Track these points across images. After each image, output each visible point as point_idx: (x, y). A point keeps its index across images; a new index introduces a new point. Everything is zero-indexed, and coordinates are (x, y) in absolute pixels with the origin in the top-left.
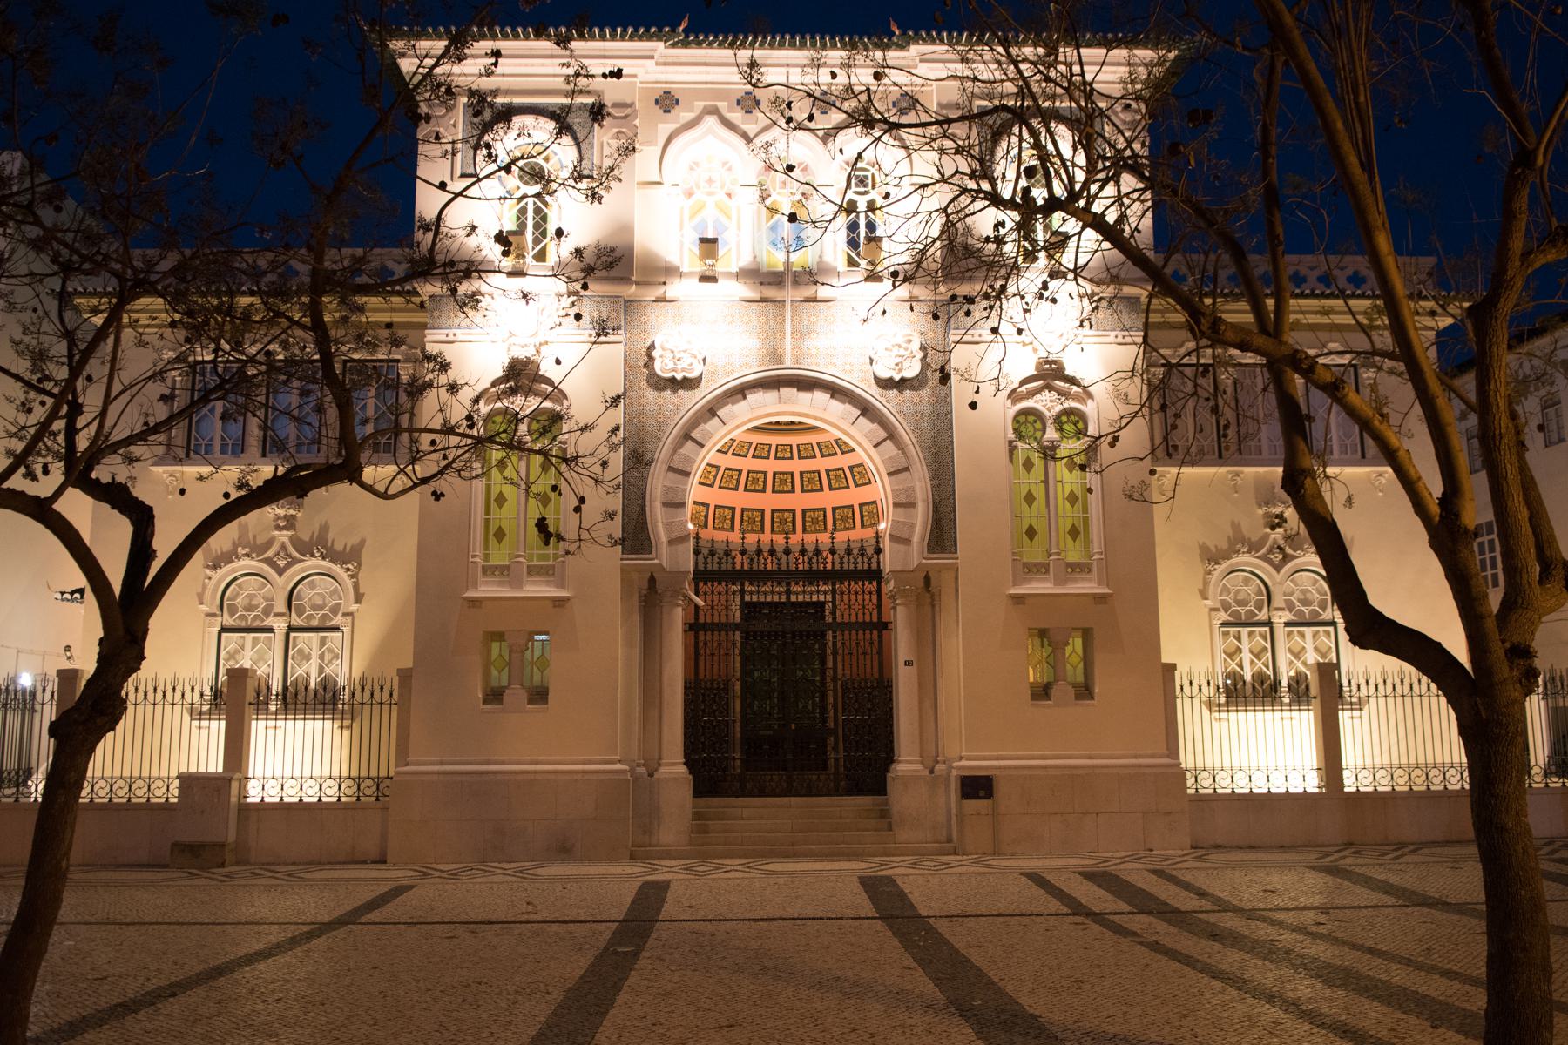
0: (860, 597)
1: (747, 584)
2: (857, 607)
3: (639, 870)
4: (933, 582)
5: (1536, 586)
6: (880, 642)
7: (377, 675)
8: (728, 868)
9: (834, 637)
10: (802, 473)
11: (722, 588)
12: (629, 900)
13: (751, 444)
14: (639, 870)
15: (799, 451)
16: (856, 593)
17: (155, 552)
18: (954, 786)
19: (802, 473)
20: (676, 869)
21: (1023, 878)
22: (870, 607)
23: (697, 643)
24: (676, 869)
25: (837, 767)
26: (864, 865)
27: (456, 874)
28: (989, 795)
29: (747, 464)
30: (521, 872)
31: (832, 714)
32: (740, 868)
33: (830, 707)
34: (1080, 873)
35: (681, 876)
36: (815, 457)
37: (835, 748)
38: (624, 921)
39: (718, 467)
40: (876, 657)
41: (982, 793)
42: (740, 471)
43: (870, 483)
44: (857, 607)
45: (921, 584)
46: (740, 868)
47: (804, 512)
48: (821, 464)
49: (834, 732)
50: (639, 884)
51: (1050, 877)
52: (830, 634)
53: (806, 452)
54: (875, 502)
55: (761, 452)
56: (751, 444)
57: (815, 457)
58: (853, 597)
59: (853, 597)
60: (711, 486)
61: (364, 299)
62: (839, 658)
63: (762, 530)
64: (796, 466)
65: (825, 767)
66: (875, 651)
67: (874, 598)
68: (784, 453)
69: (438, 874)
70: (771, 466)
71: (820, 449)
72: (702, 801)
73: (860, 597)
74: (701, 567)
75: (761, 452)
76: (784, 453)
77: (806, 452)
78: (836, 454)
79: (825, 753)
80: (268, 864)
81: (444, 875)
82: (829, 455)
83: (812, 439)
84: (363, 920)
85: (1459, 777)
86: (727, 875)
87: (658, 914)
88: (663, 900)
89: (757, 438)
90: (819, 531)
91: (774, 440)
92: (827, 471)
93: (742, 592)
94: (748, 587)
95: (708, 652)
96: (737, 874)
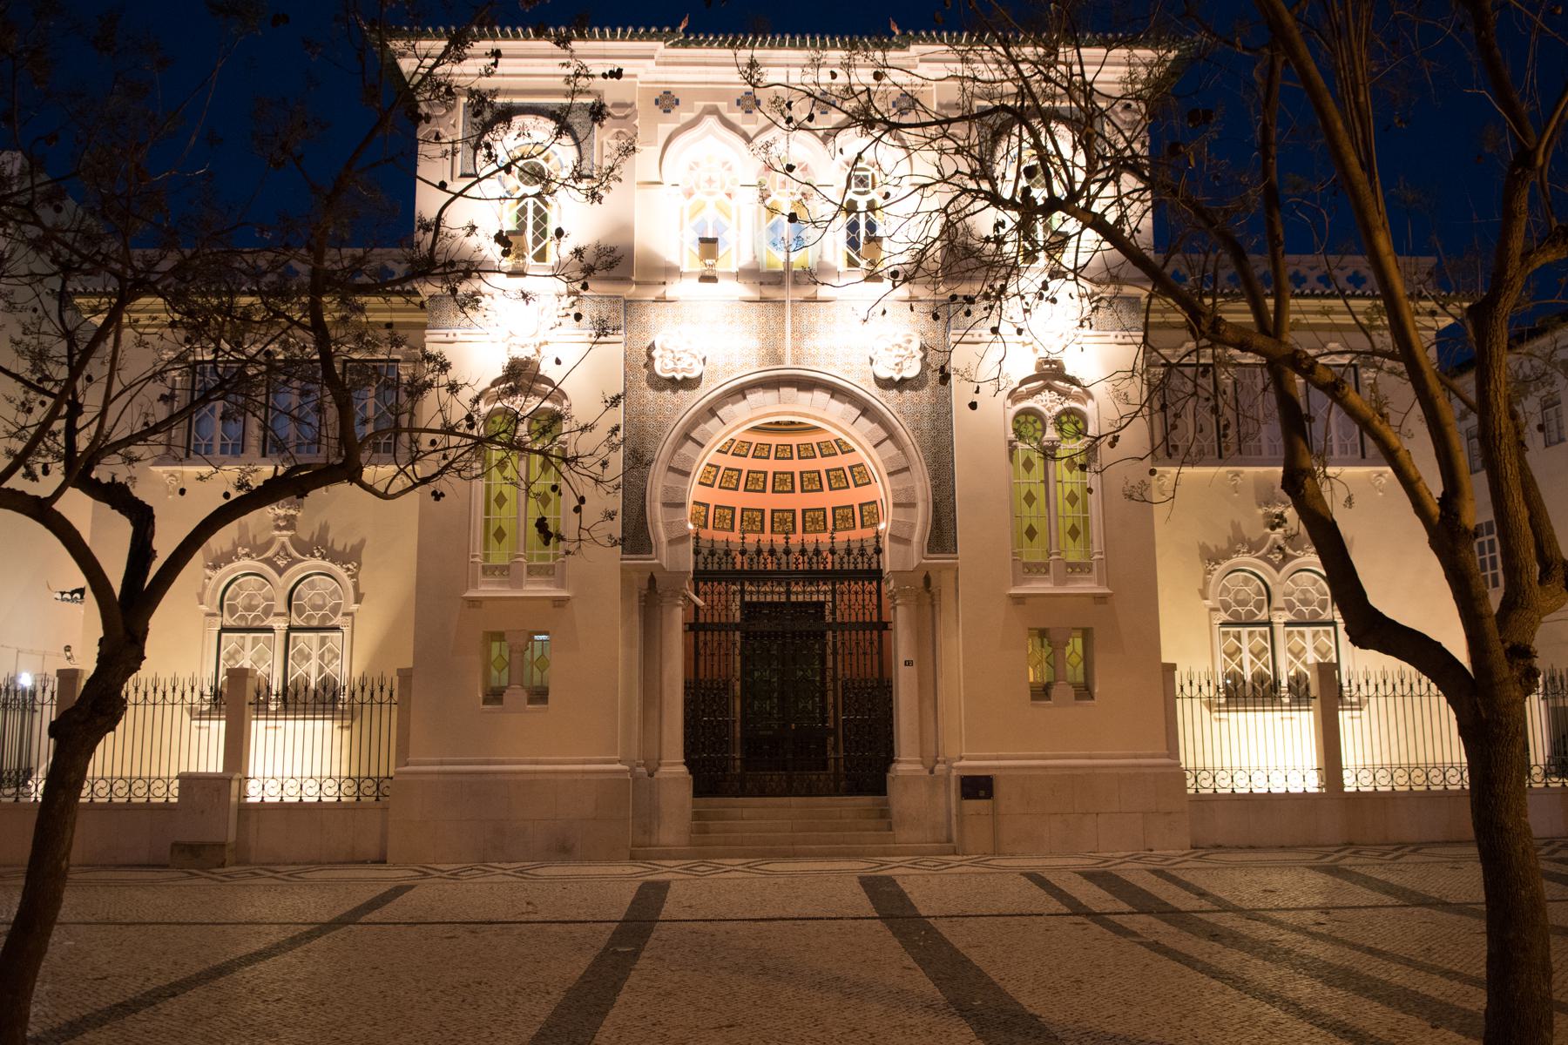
1: (747, 584)
2: (857, 607)
3: (639, 870)
4: (933, 582)
5: (1536, 586)
6: (880, 642)
7: (377, 675)
8: (728, 868)
9: (834, 637)
10: (802, 473)
12: (629, 900)
13: (751, 444)
14: (639, 870)
15: (799, 451)
16: (856, 593)
17: (155, 552)
18: (954, 786)
19: (802, 473)
20: (676, 869)
21: (1023, 878)
22: (870, 607)
23: (697, 643)
24: (676, 869)
26: (864, 865)
27: (456, 874)
28: (989, 795)
29: (747, 464)
30: (521, 872)
31: (832, 714)
32: (740, 868)
33: (830, 707)
34: (1080, 873)
35: (681, 876)
36: (815, 457)
37: (835, 748)
38: (624, 921)
39: (718, 467)
40: (876, 657)
41: (982, 793)
42: (740, 471)
43: (870, 483)
44: (857, 607)
45: (921, 584)
46: (740, 868)
47: (804, 512)
48: (821, 464)
49: (834, 732)
50: (639, 884)
51: (1050, 877)
52: (830, 634)
53: (806, 452)
54: (875, 502)
55: (761, 452)
56: (751, 444)
57: (815, 457)
59: (853, 597)
60: (711, 486)
61: (364, 299)
62: (839, 658)
63: (762, 530)
64: (796, 466)
65: (825, 767)
66: (875, 651)
67: (874, 598)
68: (784, 453)
69: (438, 874)
70: (771, 466)
71: (820, 449)
72: (702, 801)
73: (860, 597)
74: (701, 567)
75: (761, 452)
76: (784, 453)
77: (806, 452)
78: (836, 454)
79: (825, 753)
80: (268, 864)
81: (444, 875)
82: (829, 455)
83: (812, 439)
84: (363, 920)
85: (1459, 777)
86: (727, 875)
87: (658, 914)
88: (663, 900)
89: (757, 438)
91: (774, 440)
92: (827, 471)
93: (742, 592)
94: (748, 587)
95: (708, 652)
96: (737, 874)
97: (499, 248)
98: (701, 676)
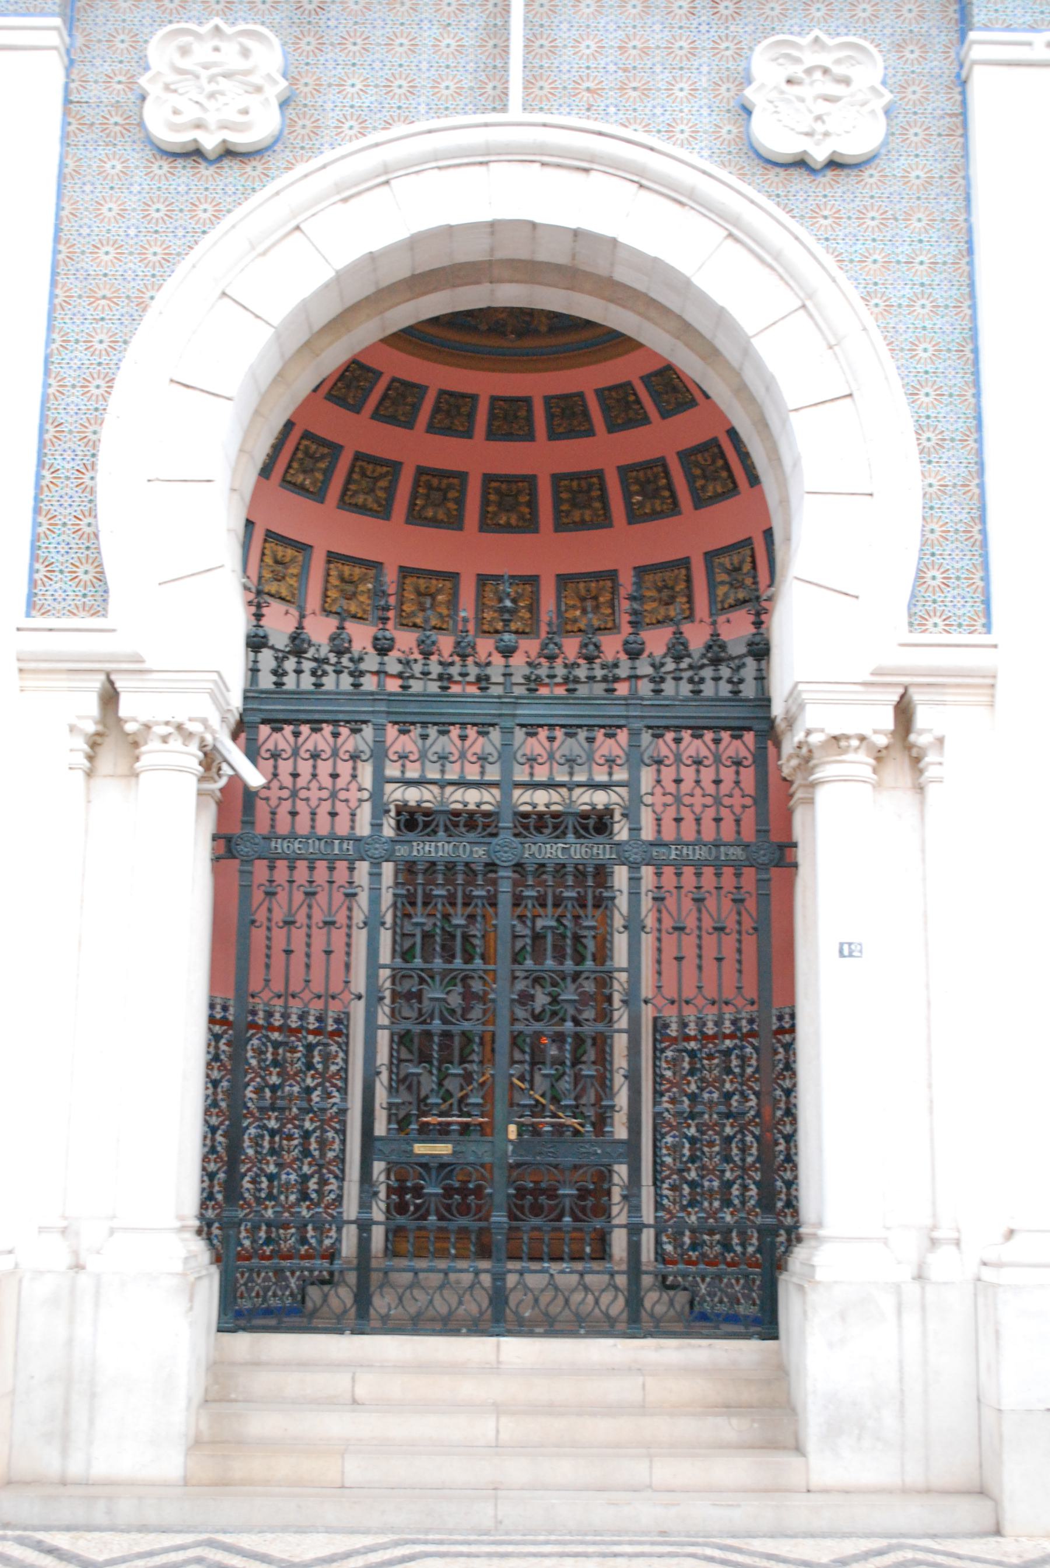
0: (324, 768)
1: (392, 731)
2: (698, 801)
5: (231, 1002)
6: (764, 898)
9: (635, 881)
11: (322, 740)
16: (315, 756)
22: (353, 795)
23: (246, 890)
25: (634, 1248)
31: (622, 1099)
33: (619, 1081)
37: (631, 1197)
40: (750, 944)
44: (314, 794)
49: (631, 1150)
52: (621, 876)
58: (345, 769)
59: (305, 768)
62: (647, 941)
65: (602, 1252)
66: (748, 924)
67: (748, 776)
72: (243, 1343)
73: (324, 768)
74: (266, 681)
79: (604, 1211)
90: (614, 591)
93: (379, 754)
94: (397, 741)
95: (318, 917)
97: (819, 123)
98: (255, 984)
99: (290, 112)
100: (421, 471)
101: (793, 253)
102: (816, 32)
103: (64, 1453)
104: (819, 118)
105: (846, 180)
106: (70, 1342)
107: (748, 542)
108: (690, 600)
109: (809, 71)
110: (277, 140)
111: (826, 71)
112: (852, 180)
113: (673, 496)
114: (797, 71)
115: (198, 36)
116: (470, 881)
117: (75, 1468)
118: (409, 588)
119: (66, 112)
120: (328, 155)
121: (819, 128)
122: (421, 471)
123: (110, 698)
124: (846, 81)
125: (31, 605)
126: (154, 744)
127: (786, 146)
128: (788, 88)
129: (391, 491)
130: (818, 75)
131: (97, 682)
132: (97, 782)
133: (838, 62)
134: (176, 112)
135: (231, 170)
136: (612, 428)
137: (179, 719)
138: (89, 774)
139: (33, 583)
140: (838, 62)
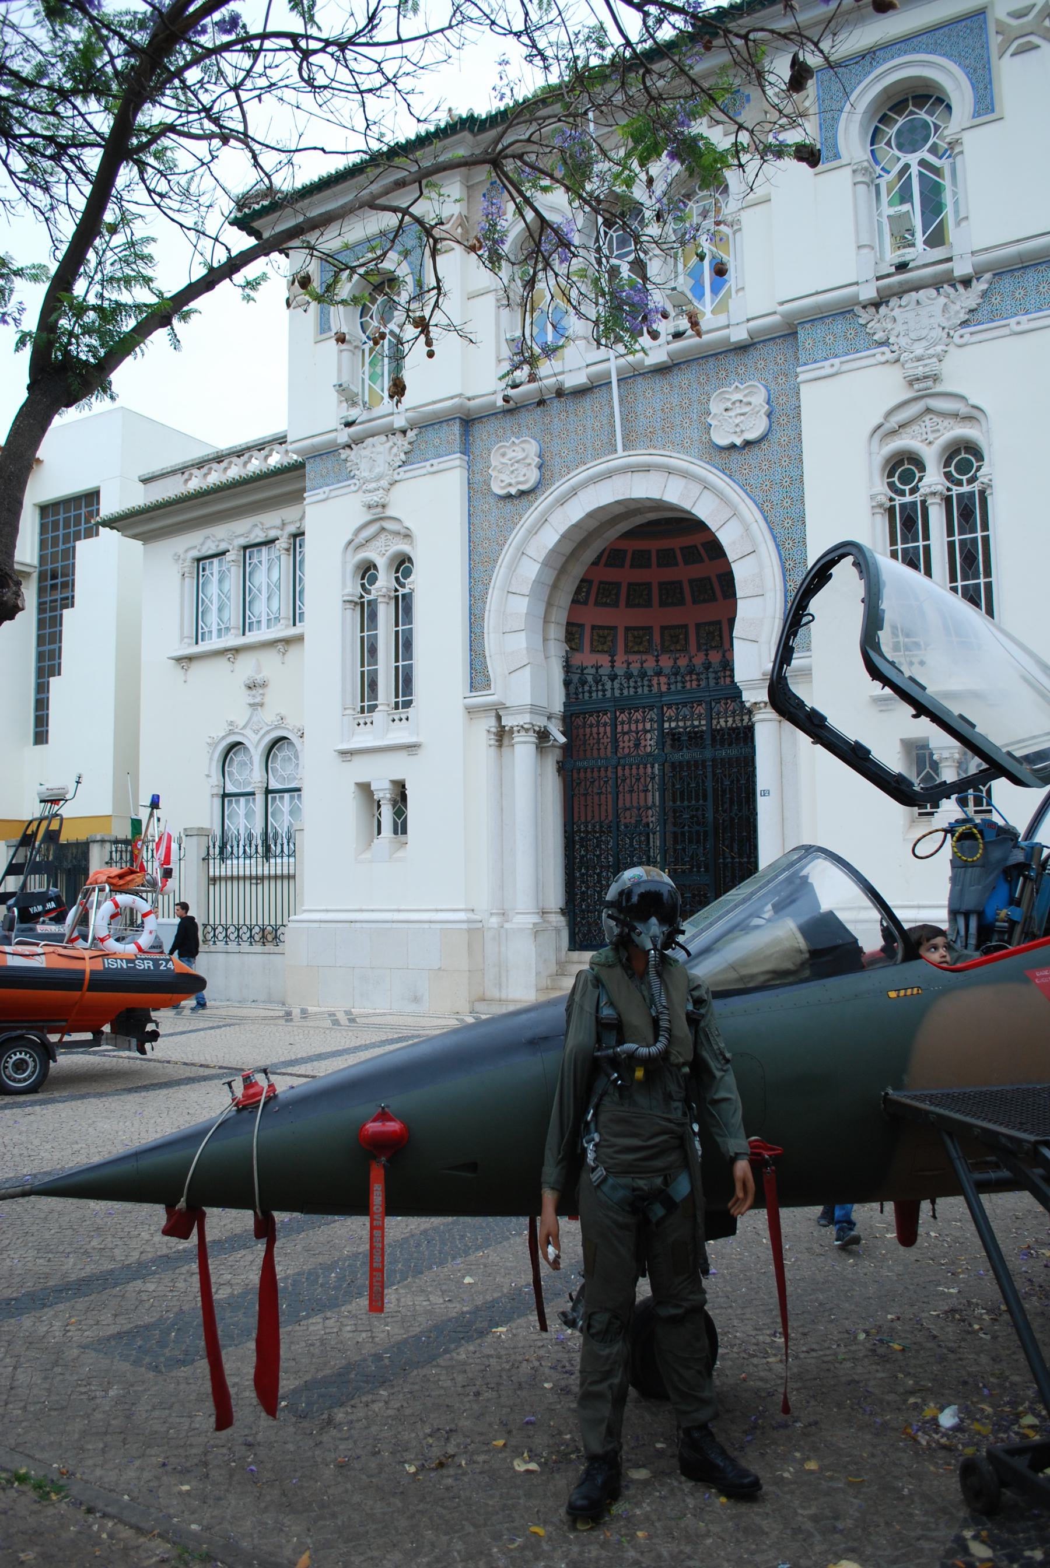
0: (595, 730)
29: (625, 575)
55: (641, 559)
68: (667, 558)
70: (655, 575)
75: (641, 559)
76: (667, 558)
91: (654, 545)
95: (627, 789)
99: (543, 470)
100: (629, 584)
101: (728, 491)
102: (736, 383)
103: (500, 991)
104: (737, 425)
105: (755, 450)
106: (499, 952)
107: (719, 623)
108: (721, 637)
109: (734, 403)
110: (539, 483)
111: (741, 401)
112: (756, 449)
113: (714, 592)
114: (729, 405)
115: (508, 447)
116: (696, 767)
117: (504, 996)
118: (630, 635)
119: (469, 488)
120: (557, 484)
121: (738, 430)
122: (629, 584)
123: (499, 718)
124: (750, 404)
125: (471, 686)
126: (516, 734)
127: (723, 442)
128: (725, 413)
129: (618, 595)
130: (738, 404)
131: (493, 713)
132: (503, 749)
133: (745, 396)
134: (502, 481)
135: (524, 501)
136: (686, 563)
137: (521, 723)
138: (500, 746)
139: (471, 678)
140: (745, 396)
